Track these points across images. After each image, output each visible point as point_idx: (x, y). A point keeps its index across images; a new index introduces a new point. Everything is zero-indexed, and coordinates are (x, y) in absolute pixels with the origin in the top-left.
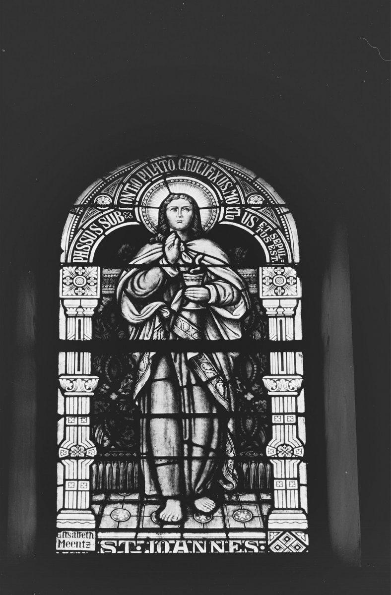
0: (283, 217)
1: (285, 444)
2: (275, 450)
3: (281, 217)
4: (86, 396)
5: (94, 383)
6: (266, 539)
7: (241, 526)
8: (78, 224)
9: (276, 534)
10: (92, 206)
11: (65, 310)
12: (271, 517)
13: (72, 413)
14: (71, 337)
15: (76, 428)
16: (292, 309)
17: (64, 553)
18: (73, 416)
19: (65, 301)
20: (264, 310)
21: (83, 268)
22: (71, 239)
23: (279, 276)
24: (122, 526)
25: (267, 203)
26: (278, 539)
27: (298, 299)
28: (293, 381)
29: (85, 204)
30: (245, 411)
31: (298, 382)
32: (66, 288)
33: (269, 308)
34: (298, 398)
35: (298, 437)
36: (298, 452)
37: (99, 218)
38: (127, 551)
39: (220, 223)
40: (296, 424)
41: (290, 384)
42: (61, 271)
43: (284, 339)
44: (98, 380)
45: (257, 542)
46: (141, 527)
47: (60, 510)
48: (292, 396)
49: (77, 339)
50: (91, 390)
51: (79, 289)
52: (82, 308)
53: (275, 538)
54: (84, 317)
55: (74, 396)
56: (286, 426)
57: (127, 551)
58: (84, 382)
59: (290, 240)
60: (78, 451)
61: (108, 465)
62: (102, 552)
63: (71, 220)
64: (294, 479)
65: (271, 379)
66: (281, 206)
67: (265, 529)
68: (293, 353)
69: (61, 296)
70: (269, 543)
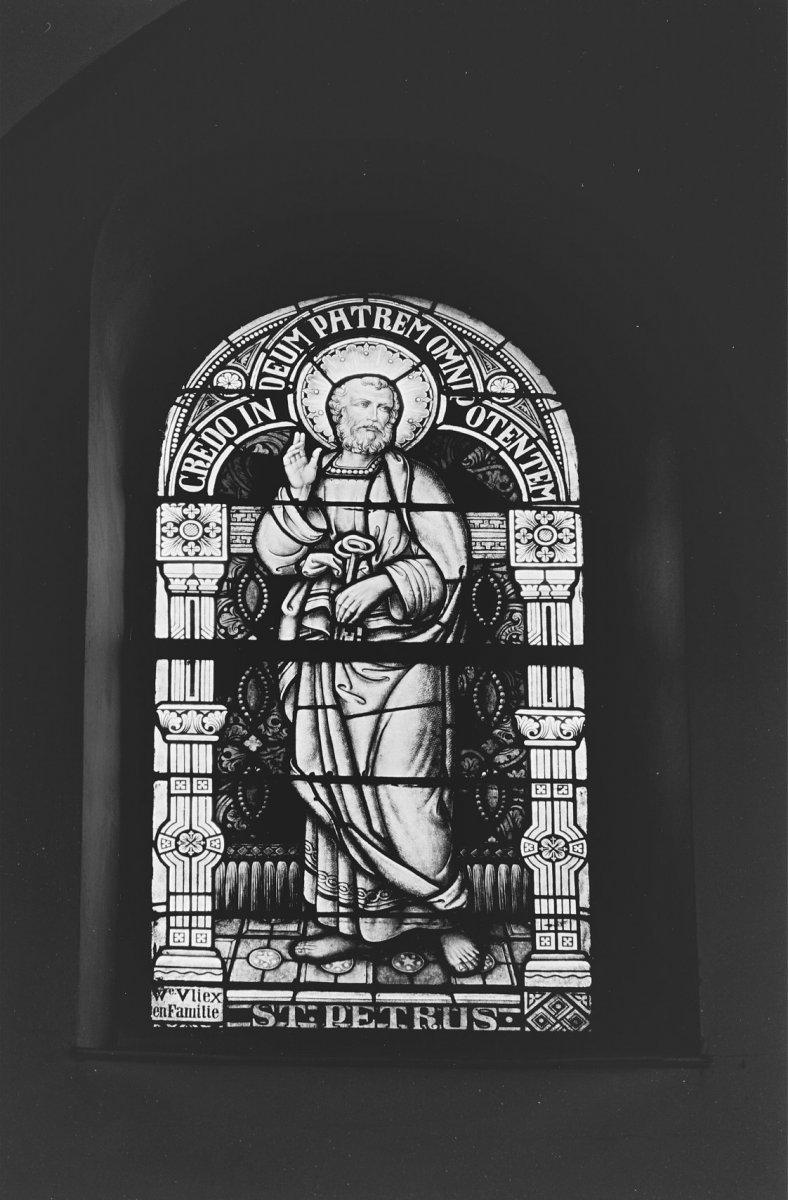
0: (550, 418)
1: (553, 834)
2: (536, 845)
3: (546, 417)
4: (206, 743)
5: (218, 717)
6: (521, 1005)
7: (331, 980)
8: (185, 424)
9: (538, 996)
10: (209, 391)
11: (167, 582)
12: (530, 965)
13: (564, 778)
14: (177, 634)
15: (549, 803)
16: (567, 587)
17: (169, 1025)
18: (543, 781)
19: (166, 566)
20: (517, 588)
21: (197, 507)
22: (173, 451)
23: (190, 522)
24: (270, 978)
25: (522, 393)
26: (540, 1005)
27: (577, 570)
28: (568, 721)
29: (197, 387)
30: (484, 774)
31: (577, 722)
32: (522, 549)
33: (526, 585)
34: (577, 751)
35: (575, 824)
36: (577, 848)
37: (216, 418)
38: (292, 1024)
39: (440, 428)
40: (574, 800)
41: (205, 720)
42: (158, 510)
43: (197, 637)
44: (225, 713)
45: (494, 1010)
46: (302, 980)
47: (162, 948)
48: (566, 748)
49: (545, 643)
50: (572, 736)
51: (189, 544)
52: (197, 578)
53: (537, 1002)
54: (200, 595)
55: (184, 742)
56: (556, 803)
57: (393, 1024)
58: (201, 716)
59: (562, 460)
60: (191, 840)
61: (489, 868)
62: (255, 1024)
63: (174, 416)
64: (570, 897)
65: (529, 716)
66: (548, 396)
67: (518, 988)
68: (568, 668)
69: (158, 558)
70: (526, 1011)
